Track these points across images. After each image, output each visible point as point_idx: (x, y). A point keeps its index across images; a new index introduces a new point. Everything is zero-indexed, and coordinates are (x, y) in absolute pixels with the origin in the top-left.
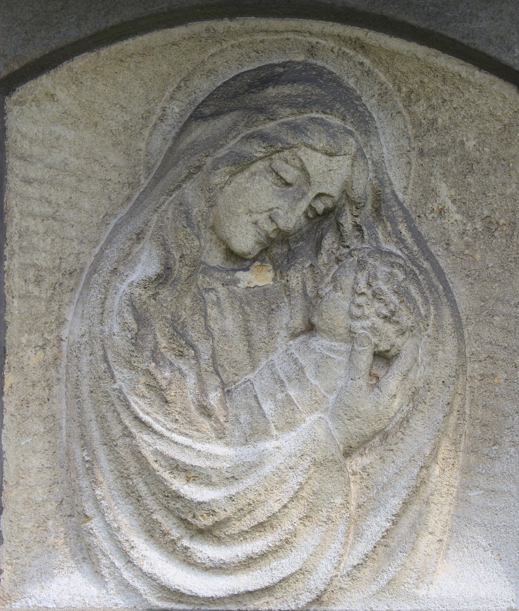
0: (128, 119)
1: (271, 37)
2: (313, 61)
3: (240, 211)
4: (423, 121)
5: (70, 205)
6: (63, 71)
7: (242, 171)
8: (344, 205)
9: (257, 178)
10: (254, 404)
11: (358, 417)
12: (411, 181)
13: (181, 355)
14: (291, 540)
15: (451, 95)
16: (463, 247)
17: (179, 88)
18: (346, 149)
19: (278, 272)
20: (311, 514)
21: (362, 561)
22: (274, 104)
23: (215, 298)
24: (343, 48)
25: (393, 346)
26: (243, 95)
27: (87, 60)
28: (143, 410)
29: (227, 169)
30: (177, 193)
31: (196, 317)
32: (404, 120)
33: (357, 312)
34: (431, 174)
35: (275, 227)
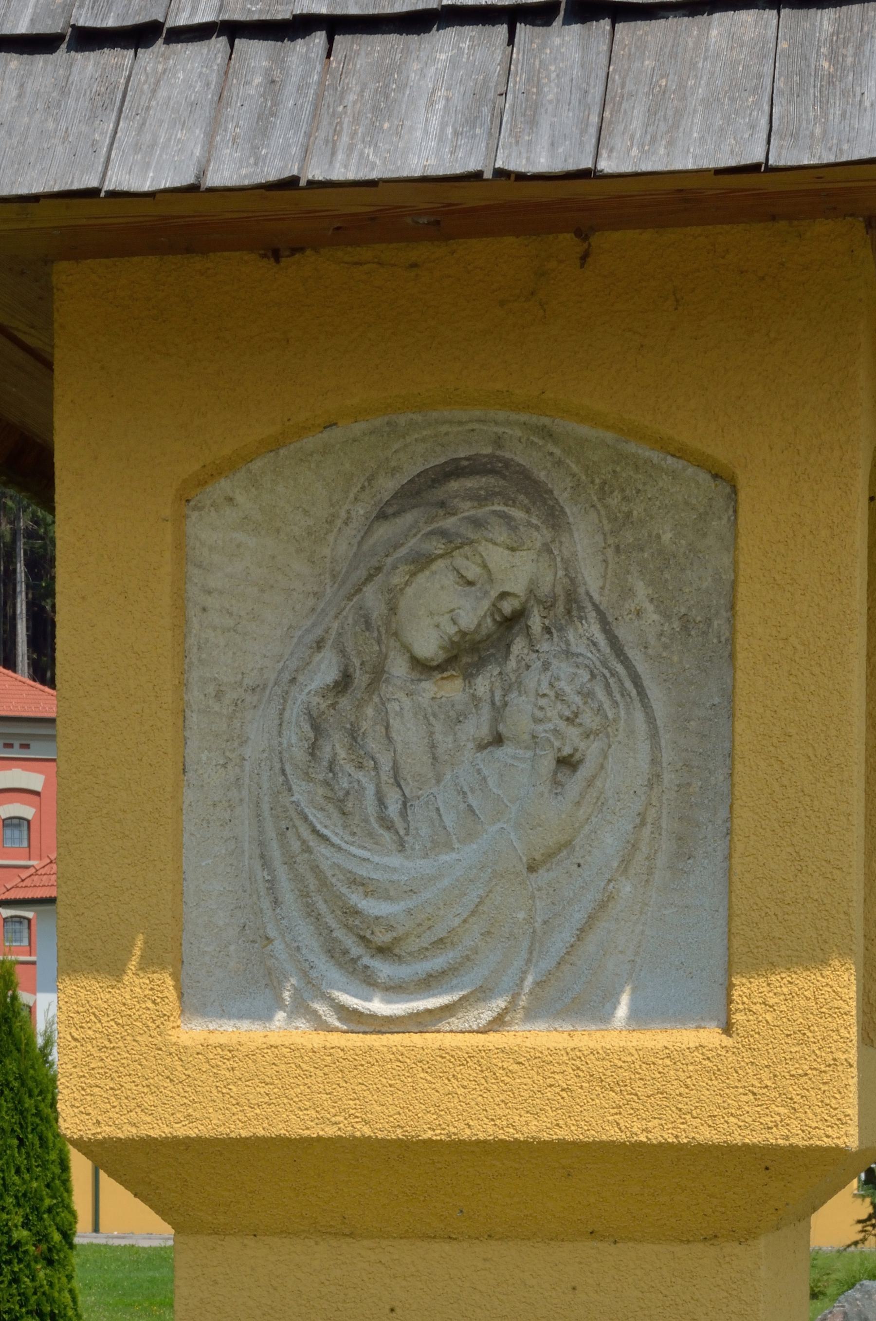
0: (312, 523)
1: (456, 429)
2: (502, 454)
3: (420, 613)
4: (618, 515)
5: (252, 616)
7: (422, 570)
8: (532, 606)
9: (438, 577)
10: (434, 815)
11: (540, 826)
12: (608, 582)
13: (360, 766)
14: (472, 957)
15: (644, 484)
16: (661, 649)
17: (363, 488)
18: (529, 543)
19: (467, 682)
20: (492, 930)
21: (544, 978)
22: (455, 498)
23: (398, 708)
24: (531, 438)
25: (576, 750)
26: (424, 490)
27: (266, 460)
28: (321, 823)
29: (406, 568)
30: (358, 597)
31: (378, 727)
32: (599, 514)
33: (539, 714)
34: (628, 572)
35: (457, 630)
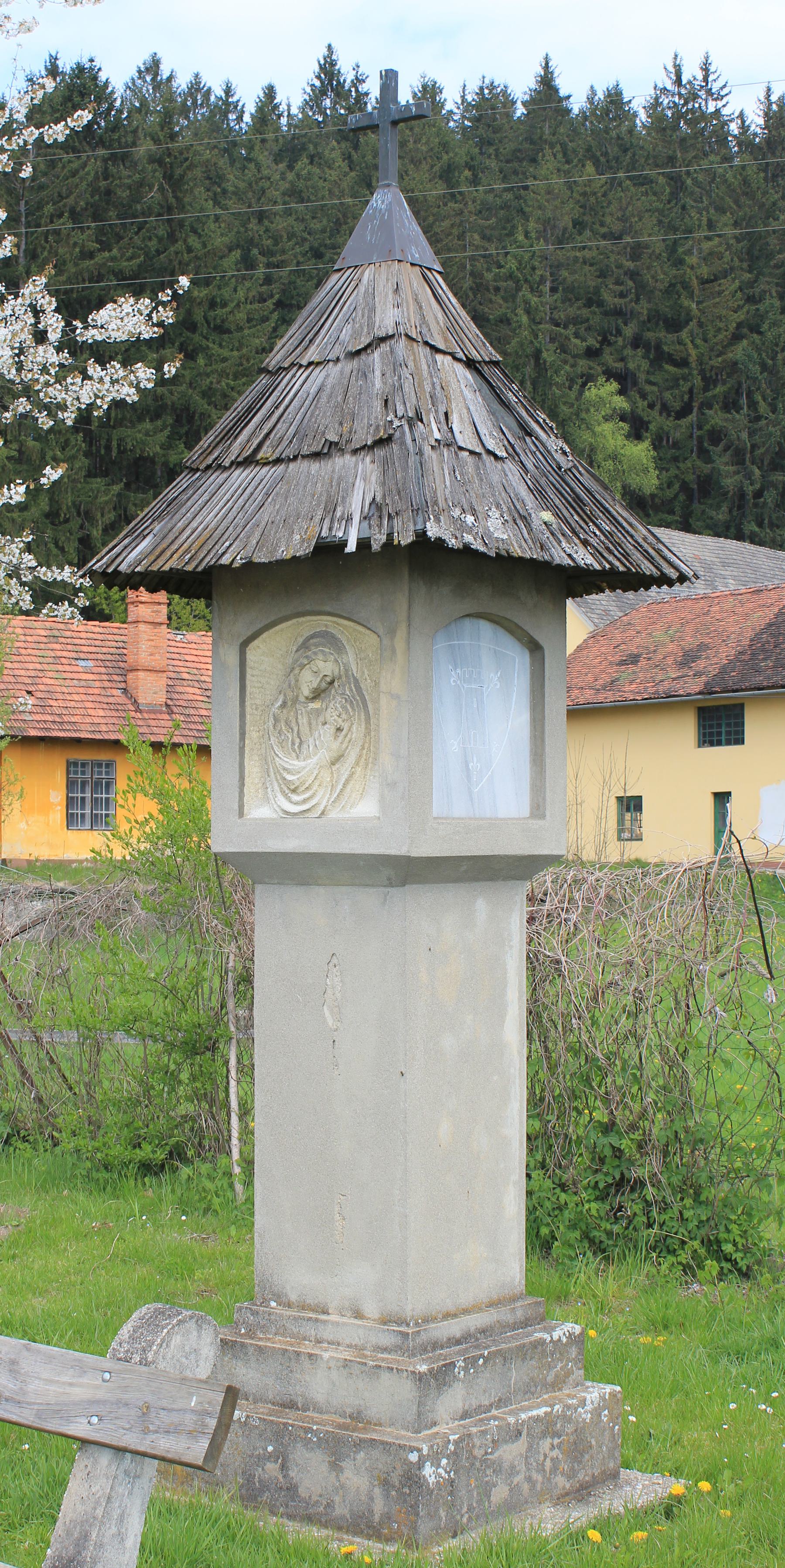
6: (260, 638)
